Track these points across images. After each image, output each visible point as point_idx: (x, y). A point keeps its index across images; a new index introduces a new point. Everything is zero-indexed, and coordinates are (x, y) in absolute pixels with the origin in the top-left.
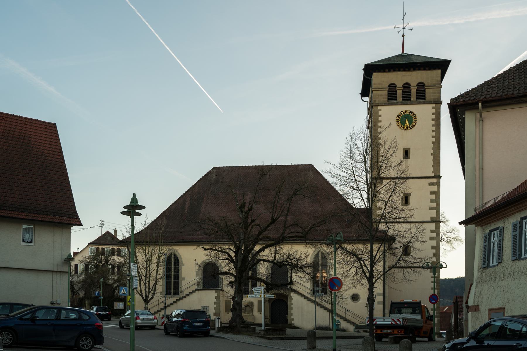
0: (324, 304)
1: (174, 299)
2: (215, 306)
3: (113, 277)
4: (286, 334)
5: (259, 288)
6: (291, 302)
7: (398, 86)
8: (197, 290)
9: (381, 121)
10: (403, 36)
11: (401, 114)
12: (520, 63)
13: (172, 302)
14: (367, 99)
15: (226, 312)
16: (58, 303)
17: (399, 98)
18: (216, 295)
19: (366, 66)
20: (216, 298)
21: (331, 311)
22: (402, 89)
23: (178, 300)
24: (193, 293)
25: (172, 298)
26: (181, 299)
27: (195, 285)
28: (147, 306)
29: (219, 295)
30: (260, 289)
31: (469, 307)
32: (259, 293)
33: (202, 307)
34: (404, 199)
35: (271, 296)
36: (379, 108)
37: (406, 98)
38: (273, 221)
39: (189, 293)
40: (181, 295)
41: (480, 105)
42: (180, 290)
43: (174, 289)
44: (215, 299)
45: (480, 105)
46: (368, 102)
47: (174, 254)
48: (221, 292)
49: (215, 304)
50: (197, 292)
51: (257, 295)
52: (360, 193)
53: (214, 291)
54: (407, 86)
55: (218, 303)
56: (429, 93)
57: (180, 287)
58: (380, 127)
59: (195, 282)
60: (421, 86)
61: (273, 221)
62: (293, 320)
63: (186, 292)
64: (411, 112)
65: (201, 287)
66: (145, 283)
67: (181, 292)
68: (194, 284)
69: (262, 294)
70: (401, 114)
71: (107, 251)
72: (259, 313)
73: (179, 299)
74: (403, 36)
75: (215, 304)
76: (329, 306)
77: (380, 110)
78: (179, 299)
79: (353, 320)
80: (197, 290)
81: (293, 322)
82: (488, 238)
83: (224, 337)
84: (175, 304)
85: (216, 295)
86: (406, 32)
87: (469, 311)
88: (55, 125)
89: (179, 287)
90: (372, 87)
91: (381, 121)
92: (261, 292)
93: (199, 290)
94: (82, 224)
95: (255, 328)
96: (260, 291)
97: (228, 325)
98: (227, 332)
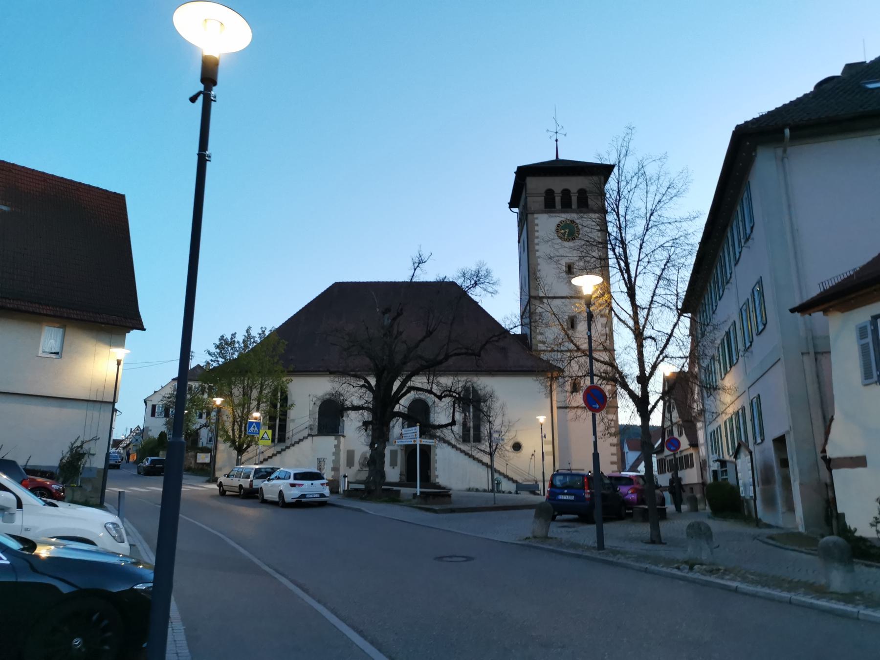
0: (479, 455)
1: (278, 448)
2: (334, 458)
3: (200, 420)
4: (450, 503)
5: (413, 430)
6: (435, 452)
7: (556, 192)
8: (309, 435)
9: (538, 231)
10: (557, 141)
11: (560, 224)
12: (849, 67)
13: (293, 443)
14: (516, 210)
15: (347, 466)
16: (91, 453)
17: (558, 205)
18: (336, 442)
19: (519, 168)
20: (335, 446)
21: (490, 467)
22: (561, 195)
23: (283, 450)
24: (287, 450)
25: (275, 448)
26: (288, 448)
27: (307, 429)
28: (240, 457)
29: (339, 442)
30: (414, 431)
31: (830, 460)
32: (412, 437)
33: (318, 459)
34: (570, 323)
35: (430, 442)
36: (536, 216)
37: (566, 205)
38: (429, 333)
39: (299, 440)
40: (288, 442)
41: (787, 131)
42: (287, 436)
43: (279, 435)
44: (334, 447)
45: (787, 131)
46: (517, 213)
47: (282, 387)
48: (342, 438)
49: (333, 455)
50: (310, 438)
51: (410, 440)
52: (528, 307)
53: (333, 438)
54: (566, 193)
55: (337, 453)
56: (592, 202)
57: (287, 431)
58: (537, 237)
59: (307, 424)
60: (582, 193)
61: (429, 333)
62: (437, 476)
63: (296, 439)
64: (573, 222)
65: (315, 432)
66: (240, 426)
67: (288, 438)
68: (306, 428)
69: (416, 438)
70: (560, 224)
71: (235, 440)
72: (392, 467)
73: (284, 448)
74: (557, 141)
75: (333, 455)
76: (486, 459)
77: (537, 218)
78: (284, 448)
79: (515, 478)
80: (309, 435)
81: (437, 480)
82: (872, 330)
83: (359, 509)
84: (279, 455)
85: (336, 442)
86: (559, 137)
87: (831, 466)
88: (122, 197)
89: (285, 432)
90: (526, 191)
91: (538, 231)
92: (416, 435)
93: (312, 436)
94: (145, 328)
95: (399, 491)
96: (414, 434)
97: (362, 487)
98: (362, 499)
